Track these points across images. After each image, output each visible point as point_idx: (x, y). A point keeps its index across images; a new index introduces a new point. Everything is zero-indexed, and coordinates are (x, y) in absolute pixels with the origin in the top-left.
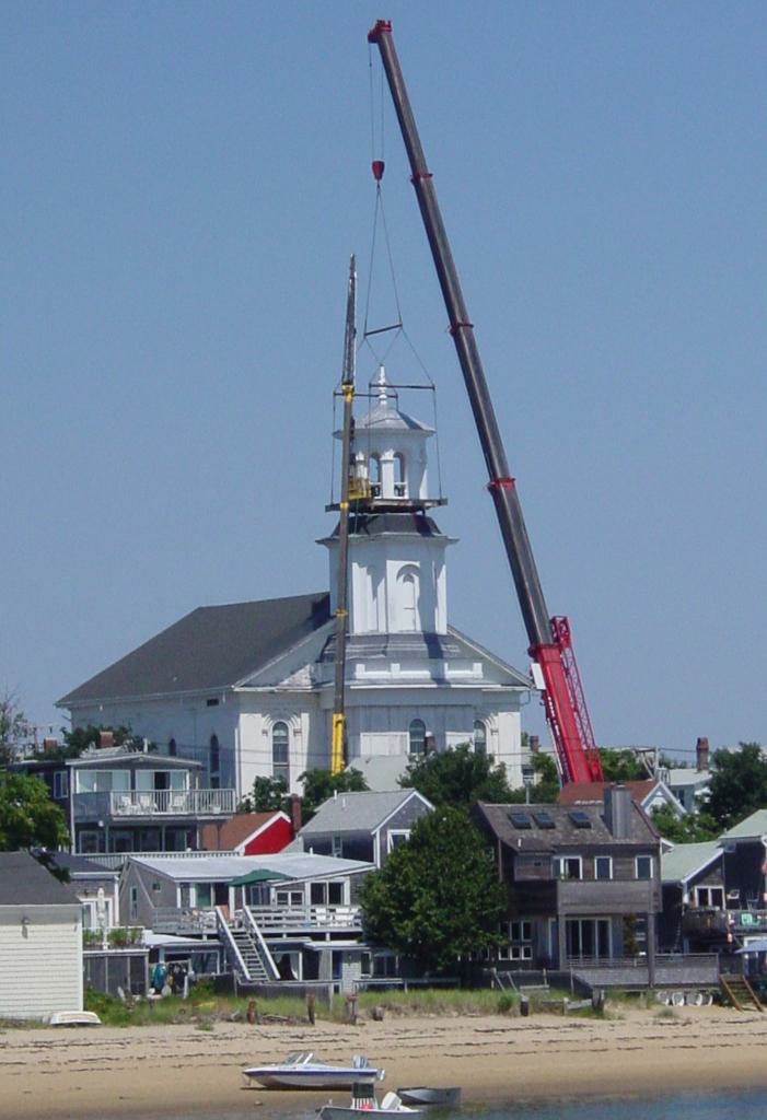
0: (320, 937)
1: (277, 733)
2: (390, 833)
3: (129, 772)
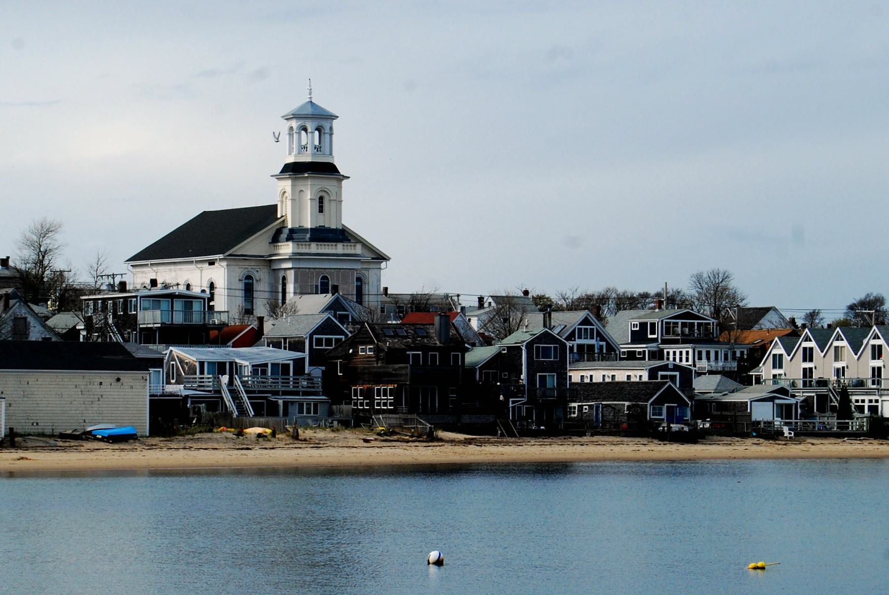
0: (276, 393)
1: (247, 281)
2: (315, 336)
3: (170, 300)
